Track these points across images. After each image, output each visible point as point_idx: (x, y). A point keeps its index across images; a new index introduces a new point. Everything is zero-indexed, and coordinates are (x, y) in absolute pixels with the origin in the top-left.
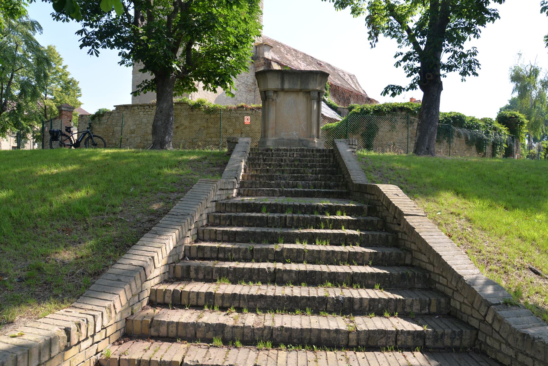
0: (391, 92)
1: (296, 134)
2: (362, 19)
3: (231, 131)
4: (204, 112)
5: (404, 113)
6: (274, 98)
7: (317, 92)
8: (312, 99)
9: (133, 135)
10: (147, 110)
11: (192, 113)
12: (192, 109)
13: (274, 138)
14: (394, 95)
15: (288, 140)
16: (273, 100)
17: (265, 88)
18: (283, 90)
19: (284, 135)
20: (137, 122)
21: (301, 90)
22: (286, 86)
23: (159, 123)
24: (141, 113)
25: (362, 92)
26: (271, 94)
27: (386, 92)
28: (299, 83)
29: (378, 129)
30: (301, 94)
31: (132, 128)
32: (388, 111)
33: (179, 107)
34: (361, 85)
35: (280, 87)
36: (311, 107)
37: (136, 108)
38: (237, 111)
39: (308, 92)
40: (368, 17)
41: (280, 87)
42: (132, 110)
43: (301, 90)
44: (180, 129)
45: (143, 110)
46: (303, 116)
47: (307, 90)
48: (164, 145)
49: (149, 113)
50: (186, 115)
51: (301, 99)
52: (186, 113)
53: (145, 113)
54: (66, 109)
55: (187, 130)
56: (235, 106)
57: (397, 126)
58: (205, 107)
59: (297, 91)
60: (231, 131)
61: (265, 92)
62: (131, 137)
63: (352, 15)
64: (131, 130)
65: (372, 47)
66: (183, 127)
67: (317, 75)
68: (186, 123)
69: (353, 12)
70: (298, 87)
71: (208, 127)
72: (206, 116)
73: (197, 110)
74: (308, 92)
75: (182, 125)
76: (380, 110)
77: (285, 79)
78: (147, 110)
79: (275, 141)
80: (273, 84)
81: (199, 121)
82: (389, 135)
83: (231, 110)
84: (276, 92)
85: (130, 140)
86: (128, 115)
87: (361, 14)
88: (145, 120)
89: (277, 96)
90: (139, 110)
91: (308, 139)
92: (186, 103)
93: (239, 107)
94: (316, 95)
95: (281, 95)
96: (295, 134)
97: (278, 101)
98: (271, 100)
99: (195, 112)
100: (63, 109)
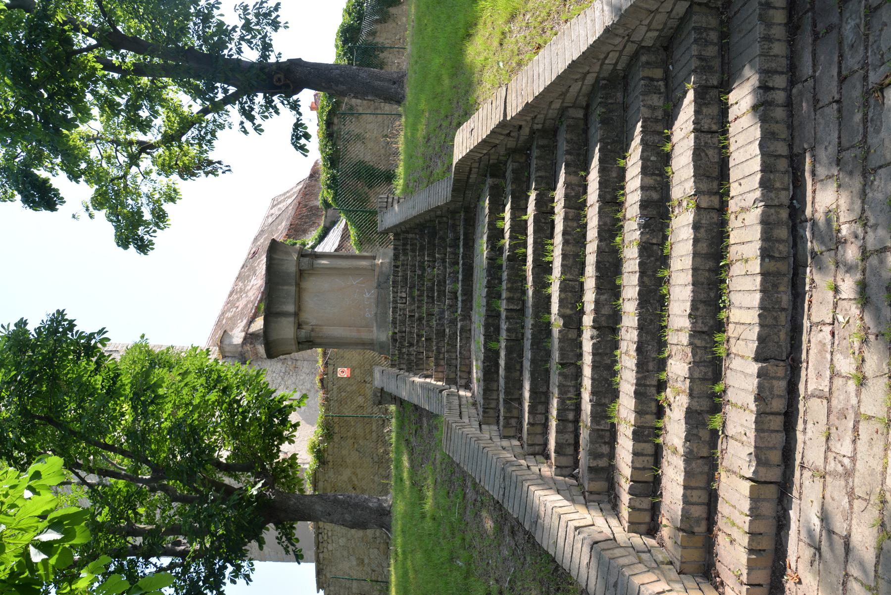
0: (303, 141)
3: (360, 400)
4: (329, 443)
5: (336, 121)
6: (308, 328)
7: (302, 259)
9: (366, 561)
10: (326, 538)
11: (331, 464)
13: (375, 328)
15: (377, 307)
16: (312, 330)
17: (293, 342)
18: (296, 314)
19: (369, 314)
20: (345, 553)
21: (298, 285)
22: (290, 308)
24: (330, 547)
25: (300, 187)
26: (303, 333)
27: (302, 149)
28: (285, 287)
29: (361, 162)
31: (355, 563)
32: (333, 145)
35: (292, 319)
37: (321, 555)
40: (182, 177)
41: (292, 319)
42: (326, 562)
43: (298, 285)
44: (356, 483)
45: (325, 545)
47: (298, 274)
48: (384, 509)
49: (330, 534)
51: (312, 285)
52: (331, 474)
55: (358, 471)
56: (321, 393)
58: (321, 442)
59: (299, 291)
60: (360, 400)
61: (299, 343)
62: (369, 564)
63: (178, 201)
64: (358, 565)
65: (229, 170)
66: (354, 479)
67: (274, 259)
68: (347, 473)
70: (292, 289)
72: (336, 440)
73: (326, 455)
74: (301, 274)
75: (350, 480)
76: (330, 159)
77: (278, 310)
78: (326, 538)
79: (379, 327)
82: (370, 145)
84: (299, 326)
86: (334, 569)
87: (176, 187)
88: (342, 541)
89: (307, 323)
90: (325, 550)
91: (376, 273)
92: (315, 473)
93: (323, 385)
94: (306, 260)
96: (367, 295)
97: (314, 322)
98: (313, 334)
99: (330, 458)
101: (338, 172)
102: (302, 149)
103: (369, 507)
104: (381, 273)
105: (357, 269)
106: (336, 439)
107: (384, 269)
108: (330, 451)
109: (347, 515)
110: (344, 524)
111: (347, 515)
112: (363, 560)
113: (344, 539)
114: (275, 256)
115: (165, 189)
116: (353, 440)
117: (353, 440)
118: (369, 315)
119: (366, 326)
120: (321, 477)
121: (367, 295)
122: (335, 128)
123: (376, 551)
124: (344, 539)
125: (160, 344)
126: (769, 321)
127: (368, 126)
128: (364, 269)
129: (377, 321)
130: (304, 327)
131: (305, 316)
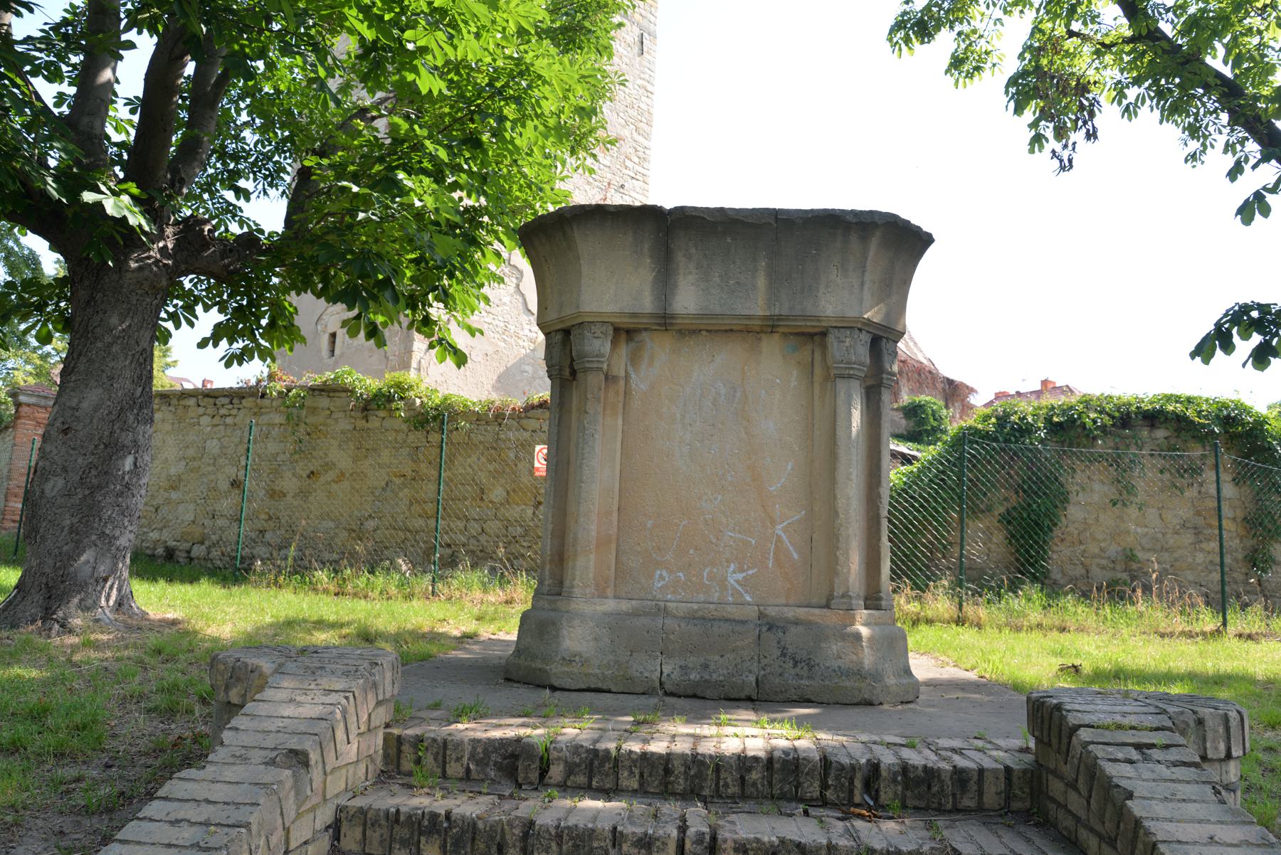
0: (1245, 346)
1: (744, 583)
2: (991, 87)
3: (497, 494)
4: (406, 420)
5: (1161, 433)
6: (620, 364)
7: (866, 338)
8: (833, 377)
9: (174, 495)
10: (223, 411)
11: (361, 424)
12: (365, 409)
13: (610, 605)
14: (1261, 357)
15: (692, 618)
16: (610, 378)
17: (568, 311)
18: (665, 321)
19: (666, 584)
20: (191, 452)
21: (771, 326)
22: (688, 299)
23: (54, 486)
24: (205, 420)
25: (925, 362)
26: (598, 345)
27: (1215, 342)
28: (761, 282)
29: (1065, 499)
30: (772, 348)
31: (173, 471)
32: (1103, 428)
33: (324, 402)
34: (920, 345)
35: (647, 304)
36: (833, 424)
37: (192, 402)
38: (524, 422)
39: (813, 337)
40: (1012, 81)
41: (647, 304)
42: (180, 410)
43: (771, 326)
44: (322, 480)
45: (211, 411)
46: (783, 473)
47: (810, 326)
48: (64, 598)
49: (229, 420)
50: (343, 432)
51: (773, 376)
52: (344, 425)
53: (217, 420)
54: (33, 400)
55: (346, 484)
56: (519, 403)
57: (1140, 485)
58: (410, 404)
59: (748, 331)
60: (497, 494)
61: (567, 332)
62: (168, 501)
63: (950, 80)
64: (169, 478)
65: (1063, 168)
66: (331, 475)
67: (864, 239)
68: (341, 458)
69: (957, 63)
70: (756, 305)
71: (416, 477)
72: (411, 437)
73: (382, 414)
74: (813, 337)
75: (328, 466)
76: (1072, 421)
77: (680, 257)
78: (223, 411)
79: (615, 623)
80: (615, 285)
81: (386, 456)
82: (1108, 519)
83: (499, 416)
84: (625, 332)
85: (164, 511)
86: (167, 427)
87: (986, 74)
88: (213, 446)
89: (634, 359)
90: (201, 410)
91: (816, 614)
92: (346, 390)
93: (533, 407)
94: (862, 353)
95: (659, 349)
96: (734, 578)
97: (640, 383)
98: (594, 380)
99: (374, 423)
100: (22, 398)
101: (1042, 441)
102: (1215, 342)
103: (78, 550)
104: (818, 634)
105: (833, 540)
106: (416, 437)
107: (835, 647)
108: (389, 423)
109: (60, 482)
110: (38, 474)
111: (60, 482)
112: (174, 488)
113: (216, 451)
114: (874, 243)
115: (982, 45)
116: (409, 474)
117: (409, 474)
118: (660, 580)
119: (621, 573)
120: (338, 402)
121: (734, 578)
122: (1145, 433)
123: (190, 517)
124: (216, 451)
125: (654, 123)
126: (729, 778)
127: (1152, 513)
128: (833, 566)
129: (635, 614)
130: (624, 350)
131: (660, 355)
